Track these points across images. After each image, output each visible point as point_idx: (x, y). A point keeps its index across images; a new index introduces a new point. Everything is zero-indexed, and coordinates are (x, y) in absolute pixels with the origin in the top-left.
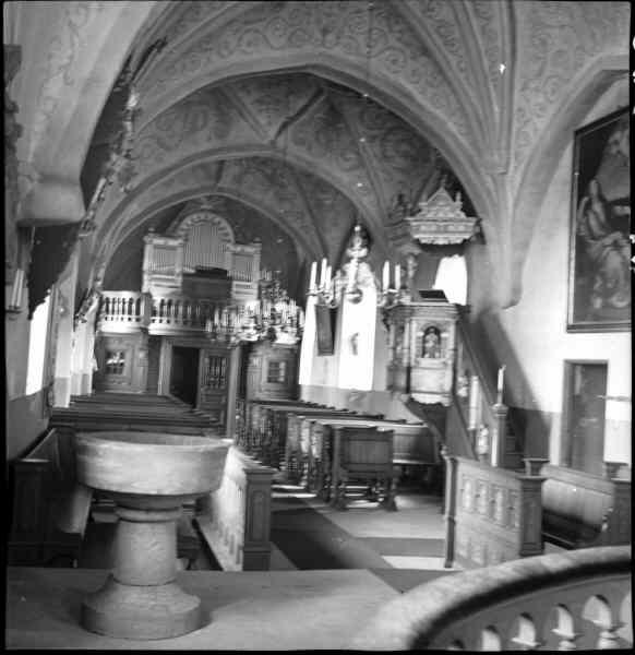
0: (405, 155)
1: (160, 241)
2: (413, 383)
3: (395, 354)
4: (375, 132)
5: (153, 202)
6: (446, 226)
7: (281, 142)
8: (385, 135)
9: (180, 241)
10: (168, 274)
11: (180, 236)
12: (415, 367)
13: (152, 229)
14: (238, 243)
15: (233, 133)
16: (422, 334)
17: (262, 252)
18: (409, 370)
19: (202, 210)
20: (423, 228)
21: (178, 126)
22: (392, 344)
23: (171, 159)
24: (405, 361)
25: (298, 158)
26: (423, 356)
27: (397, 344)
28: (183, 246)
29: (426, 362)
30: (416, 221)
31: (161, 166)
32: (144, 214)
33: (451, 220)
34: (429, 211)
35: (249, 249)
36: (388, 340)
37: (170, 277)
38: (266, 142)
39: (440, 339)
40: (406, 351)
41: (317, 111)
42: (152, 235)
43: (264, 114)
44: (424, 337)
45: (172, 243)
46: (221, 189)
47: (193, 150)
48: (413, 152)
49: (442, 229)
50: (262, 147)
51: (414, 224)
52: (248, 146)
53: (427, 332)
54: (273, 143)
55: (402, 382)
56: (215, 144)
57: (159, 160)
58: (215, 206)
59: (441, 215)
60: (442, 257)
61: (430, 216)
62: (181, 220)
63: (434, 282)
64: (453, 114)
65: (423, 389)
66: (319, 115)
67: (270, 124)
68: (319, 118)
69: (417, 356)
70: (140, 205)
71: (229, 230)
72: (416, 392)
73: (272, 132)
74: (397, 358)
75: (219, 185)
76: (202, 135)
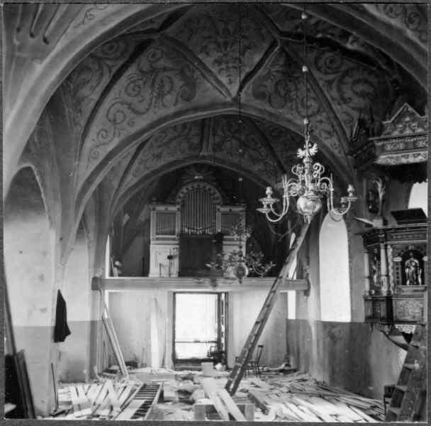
0: (362, 95)
2: (396, 313)
3: (372, 286)
4: (331, 77)
6: (415, 142)
8: (343, 77)
9: (178, 206)
10: (170, 234)
11: (178, 203)
12: (397, 296)
13: (154, 199)
14: (225, 204)
15: (199, 93)
18: (389, 299)
20: (389, 147)
21: (147, 93)
22: (367, 273)
23: (142, 123)
24: (384, 290)
26: (404, 283)
27: (372, 272)
28: (182, 210)
29: (408, 289)
30: (380, 140)
31: (133, 130)
33: (420, 135)
35: (236, 209)
36: (429, 409)
38: (229, 99)
40: (384, 278)
41: (274, 64)
42: (155, 203)
43: (224, 73)
44: (403, 263)
45: (173, 209)
47: (162, 112)
49: (411, 146)
50: (225, 104)
52: (213, 105)
54: (236, 101)
57: (131, 124)
59: (408, 132)
60: (415, 182)
61: (396, 133)
63: (407, 201)
64: (412, 22)
65: (409, 318)
66: (277, 68)
67: (230, 82)
68: (277, 71)
69: (397, 283)
70: (135, 176)
73: (234, 89)
74: (321, 54)
75: (201, 154)
76: (169, 98)
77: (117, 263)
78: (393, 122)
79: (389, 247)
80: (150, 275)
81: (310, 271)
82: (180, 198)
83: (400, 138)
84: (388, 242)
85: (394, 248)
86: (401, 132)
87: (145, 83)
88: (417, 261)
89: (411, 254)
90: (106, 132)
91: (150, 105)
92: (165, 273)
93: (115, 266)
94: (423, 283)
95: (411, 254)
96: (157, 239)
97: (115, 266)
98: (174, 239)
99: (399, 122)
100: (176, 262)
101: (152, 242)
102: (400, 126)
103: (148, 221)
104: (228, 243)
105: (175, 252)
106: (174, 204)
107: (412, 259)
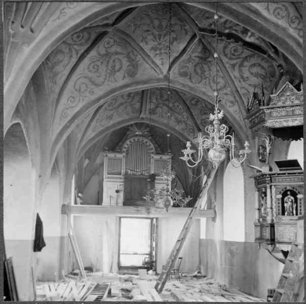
1: (111, 155)
2: (277, 236)
3: (260, 216)
4: (234, 62)
5: (102, 128)
7: (171, 76)
9: (124, 154)
15: (140, 72)
16: (280, 196)
17: (172, 158)
18: (272, 226)
19: (137, 135)
20: (275, 114)
21: (103, 69)
25: (184, 85)
27: (261, 205)
28: (126, 157)
32: (97, 135)
34: (279, 101)
35: (165, 157)
37: (118, 176)
38: (161, 76)
39: (296, 199)
40: (269, 210)
45: (119, 156)
46: (143, 119)
48: (262, 72)
50: (159, 80)
51: (268, 111)
53: (285, 194)
54: (167, 78)
55: (267, 234)
56: (127, 80)
58: (206, 174)
59: (288, 103)
60: (293, 140)
61: (280, 104)
62: (124, 143)
63: (286, 154)
65: (286, 240)
66: (197, 54)
68: (196, 57)
71: (152, 146)
72: (280, 243)
74: (263, 217)
76: (119, 75)
77: (80, 195)
78: (278, 95)
79: (273, 187)
80: (103, 204)
81: (217, 204)
82: (125, 148)
83: (283, 107)
84: (272, 184)
85: (277, 188)
86: (284, 103)
87: (102, 63)
88: (292, 198)
89: (289, 193)
90: (74, 98)
91: (105, 79)
92: (113, 202)
93: (78, 197)
94: (297, 214)
95: (289, 193)
96: (108, 178)
97: (78, 197)
98: (120, 178)
99: (282, 95)
100: (122, 194)
101: (105, 180)
102: (283, 99)
103: (102, 165)
104: (158, 182)
105: (122, 188)
106: (121, 152)
107: (289, 196)
